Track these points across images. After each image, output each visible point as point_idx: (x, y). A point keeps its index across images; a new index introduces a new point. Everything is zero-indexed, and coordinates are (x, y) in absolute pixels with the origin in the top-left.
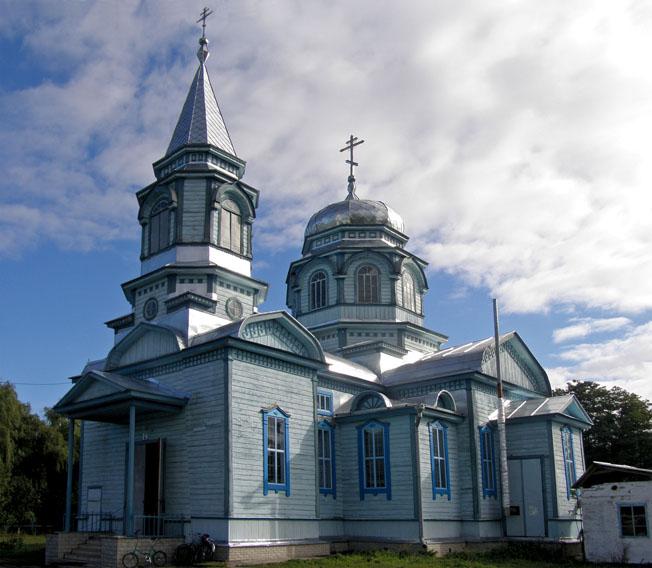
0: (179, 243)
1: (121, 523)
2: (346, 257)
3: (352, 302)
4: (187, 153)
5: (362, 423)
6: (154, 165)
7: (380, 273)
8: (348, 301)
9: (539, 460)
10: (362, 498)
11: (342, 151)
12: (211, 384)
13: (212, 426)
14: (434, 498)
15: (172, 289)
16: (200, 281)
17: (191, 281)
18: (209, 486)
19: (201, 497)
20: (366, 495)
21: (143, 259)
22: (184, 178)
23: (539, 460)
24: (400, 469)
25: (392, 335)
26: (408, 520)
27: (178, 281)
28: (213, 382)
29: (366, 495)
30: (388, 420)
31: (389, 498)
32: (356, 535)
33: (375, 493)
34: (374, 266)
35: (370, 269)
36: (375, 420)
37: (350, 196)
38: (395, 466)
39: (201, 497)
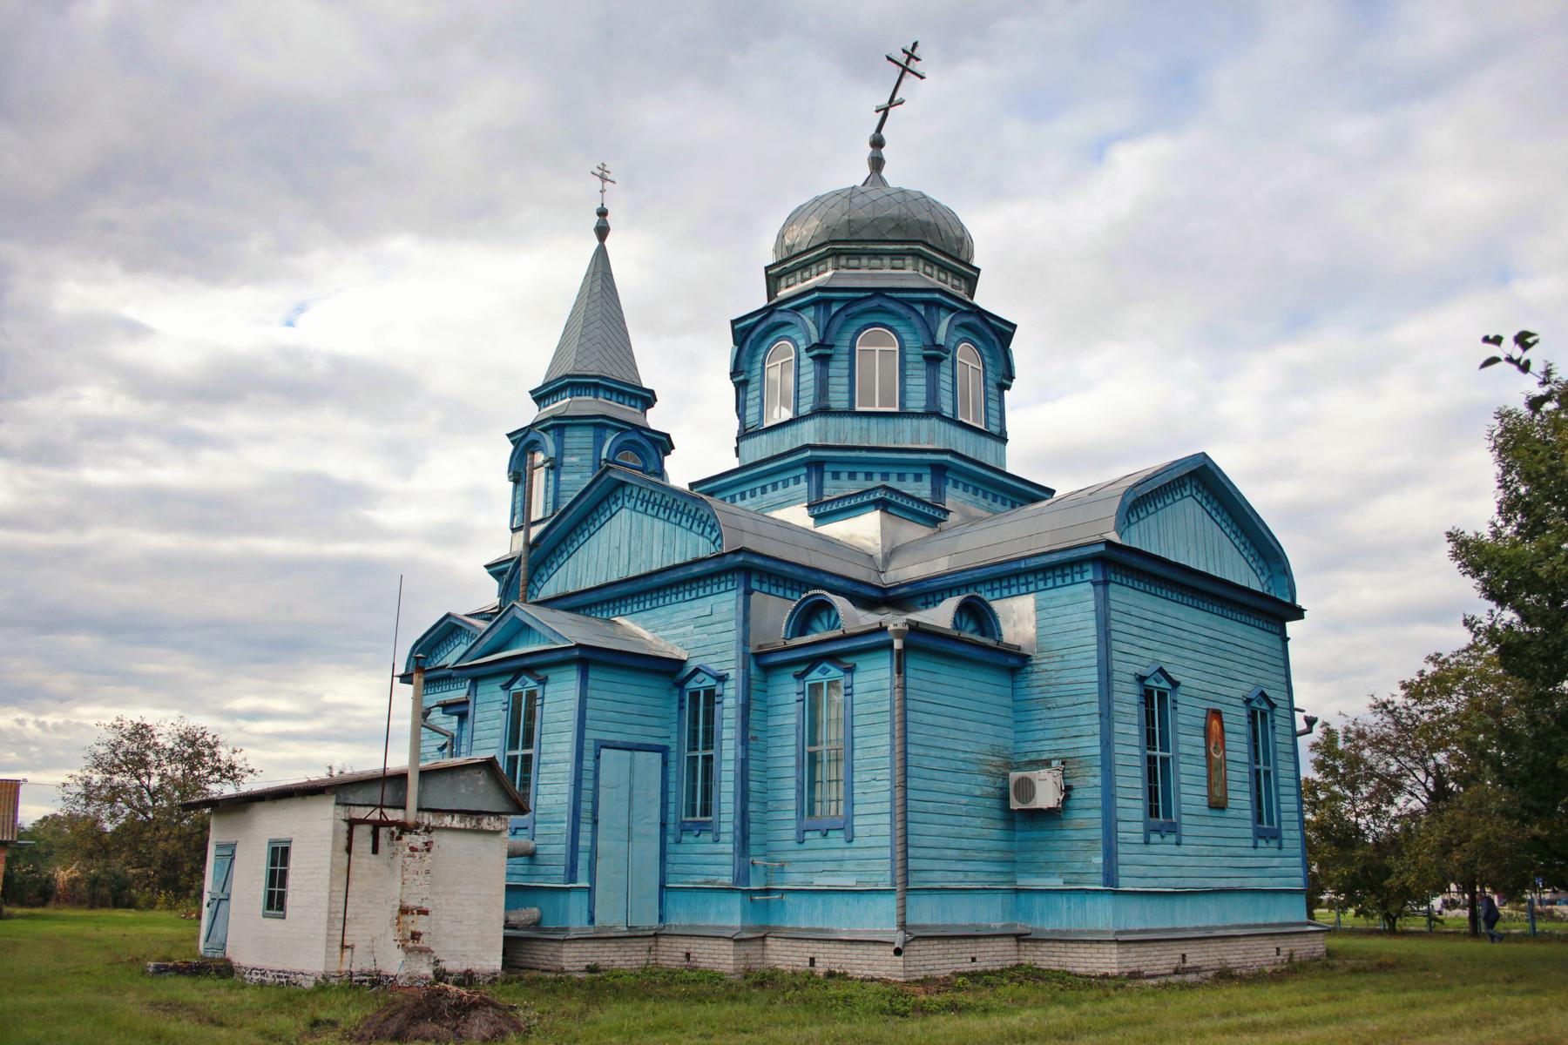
2: (834, 309)
8: (834, 405)
25: (918, 477)
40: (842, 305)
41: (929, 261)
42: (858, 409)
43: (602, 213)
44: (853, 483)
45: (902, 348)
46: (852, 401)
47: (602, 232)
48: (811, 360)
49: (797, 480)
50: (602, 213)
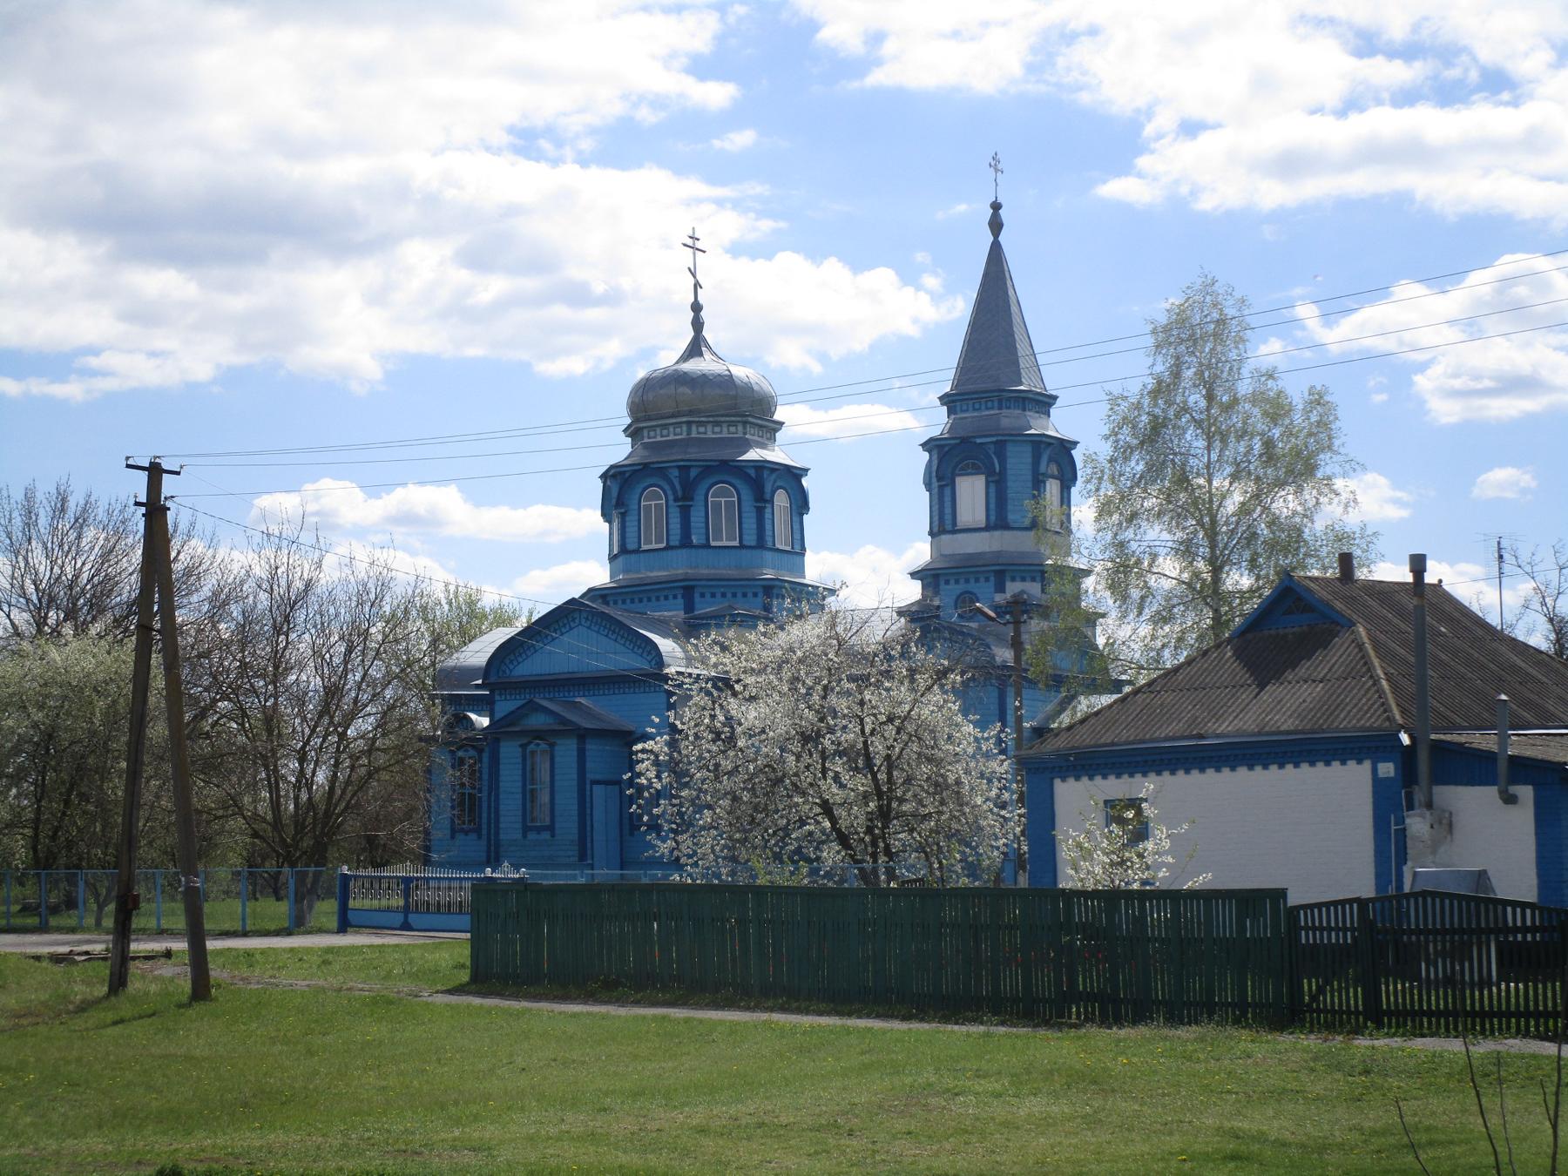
3: (753, 543)
10: (453, 837)
11: (704, 252)
14: (453, 837)
33: (466, 833)
37: (696, 347)
40: (700, 469)
42: (644, 547)
43: (996, 207)
45: (739, 499)
46: (708, 539)
47: (996, 225)
48: (678, 509)
49: (675, 597)
50: (996, 207)
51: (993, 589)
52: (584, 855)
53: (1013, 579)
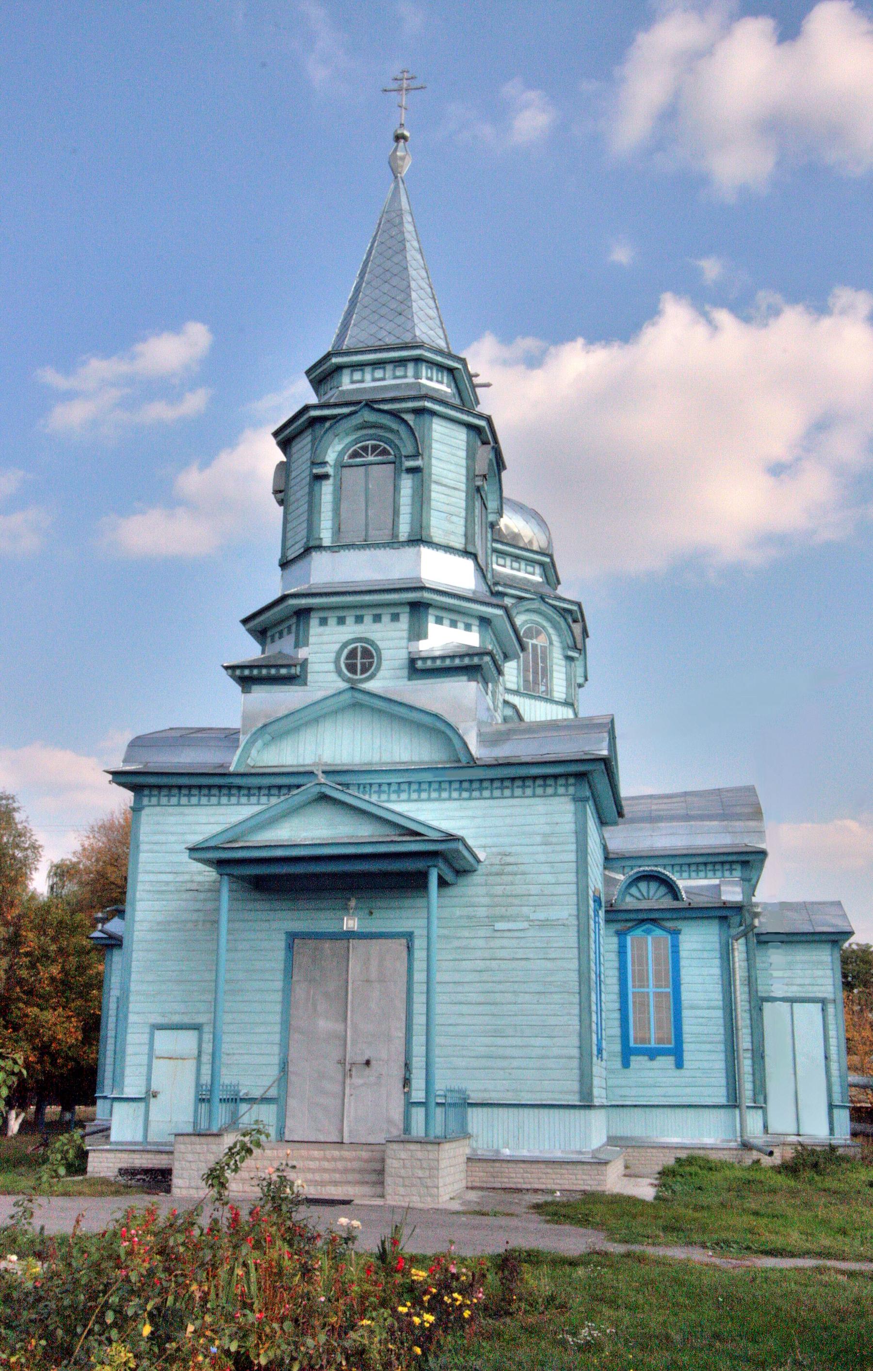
0: (419, 539)
1: (273, 1108)
4: (417, 360)
5: (629, 924)
6: (308, 373)
7: (551, 643)
9: (820, 1005)
10: (626, 1064)
12: (538, 839)
13: (545, 924)
15: (418, 633)
16: (395, 617)
17: (359, 619)
18: (538, 1041)
19: (515, 1063)
20: (632, 1058)
21: (284, 564)
22: (433, 413)
23: (820, 1005)
24: (699, 1013)
26: (714, 1107)
27: (431, 619)
28: (544, 835)
29: (632, 1058)
30: (679, 924)
31: (679, 1065)
32: (633, 1135)
34: (543, 627)
35: (538, 633)
36: (653, 921)
38: (692, 1008)
39: (515, 1063)
41: (517, 558)
44: (342, 629)
51: (405, 634)
52: (226, 981)
53: (439, 621)
